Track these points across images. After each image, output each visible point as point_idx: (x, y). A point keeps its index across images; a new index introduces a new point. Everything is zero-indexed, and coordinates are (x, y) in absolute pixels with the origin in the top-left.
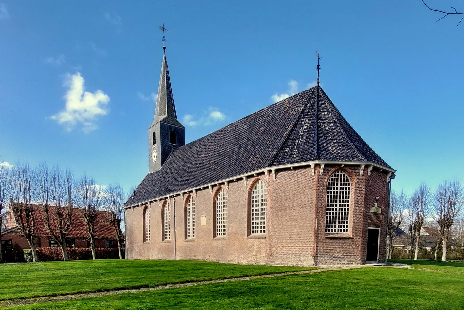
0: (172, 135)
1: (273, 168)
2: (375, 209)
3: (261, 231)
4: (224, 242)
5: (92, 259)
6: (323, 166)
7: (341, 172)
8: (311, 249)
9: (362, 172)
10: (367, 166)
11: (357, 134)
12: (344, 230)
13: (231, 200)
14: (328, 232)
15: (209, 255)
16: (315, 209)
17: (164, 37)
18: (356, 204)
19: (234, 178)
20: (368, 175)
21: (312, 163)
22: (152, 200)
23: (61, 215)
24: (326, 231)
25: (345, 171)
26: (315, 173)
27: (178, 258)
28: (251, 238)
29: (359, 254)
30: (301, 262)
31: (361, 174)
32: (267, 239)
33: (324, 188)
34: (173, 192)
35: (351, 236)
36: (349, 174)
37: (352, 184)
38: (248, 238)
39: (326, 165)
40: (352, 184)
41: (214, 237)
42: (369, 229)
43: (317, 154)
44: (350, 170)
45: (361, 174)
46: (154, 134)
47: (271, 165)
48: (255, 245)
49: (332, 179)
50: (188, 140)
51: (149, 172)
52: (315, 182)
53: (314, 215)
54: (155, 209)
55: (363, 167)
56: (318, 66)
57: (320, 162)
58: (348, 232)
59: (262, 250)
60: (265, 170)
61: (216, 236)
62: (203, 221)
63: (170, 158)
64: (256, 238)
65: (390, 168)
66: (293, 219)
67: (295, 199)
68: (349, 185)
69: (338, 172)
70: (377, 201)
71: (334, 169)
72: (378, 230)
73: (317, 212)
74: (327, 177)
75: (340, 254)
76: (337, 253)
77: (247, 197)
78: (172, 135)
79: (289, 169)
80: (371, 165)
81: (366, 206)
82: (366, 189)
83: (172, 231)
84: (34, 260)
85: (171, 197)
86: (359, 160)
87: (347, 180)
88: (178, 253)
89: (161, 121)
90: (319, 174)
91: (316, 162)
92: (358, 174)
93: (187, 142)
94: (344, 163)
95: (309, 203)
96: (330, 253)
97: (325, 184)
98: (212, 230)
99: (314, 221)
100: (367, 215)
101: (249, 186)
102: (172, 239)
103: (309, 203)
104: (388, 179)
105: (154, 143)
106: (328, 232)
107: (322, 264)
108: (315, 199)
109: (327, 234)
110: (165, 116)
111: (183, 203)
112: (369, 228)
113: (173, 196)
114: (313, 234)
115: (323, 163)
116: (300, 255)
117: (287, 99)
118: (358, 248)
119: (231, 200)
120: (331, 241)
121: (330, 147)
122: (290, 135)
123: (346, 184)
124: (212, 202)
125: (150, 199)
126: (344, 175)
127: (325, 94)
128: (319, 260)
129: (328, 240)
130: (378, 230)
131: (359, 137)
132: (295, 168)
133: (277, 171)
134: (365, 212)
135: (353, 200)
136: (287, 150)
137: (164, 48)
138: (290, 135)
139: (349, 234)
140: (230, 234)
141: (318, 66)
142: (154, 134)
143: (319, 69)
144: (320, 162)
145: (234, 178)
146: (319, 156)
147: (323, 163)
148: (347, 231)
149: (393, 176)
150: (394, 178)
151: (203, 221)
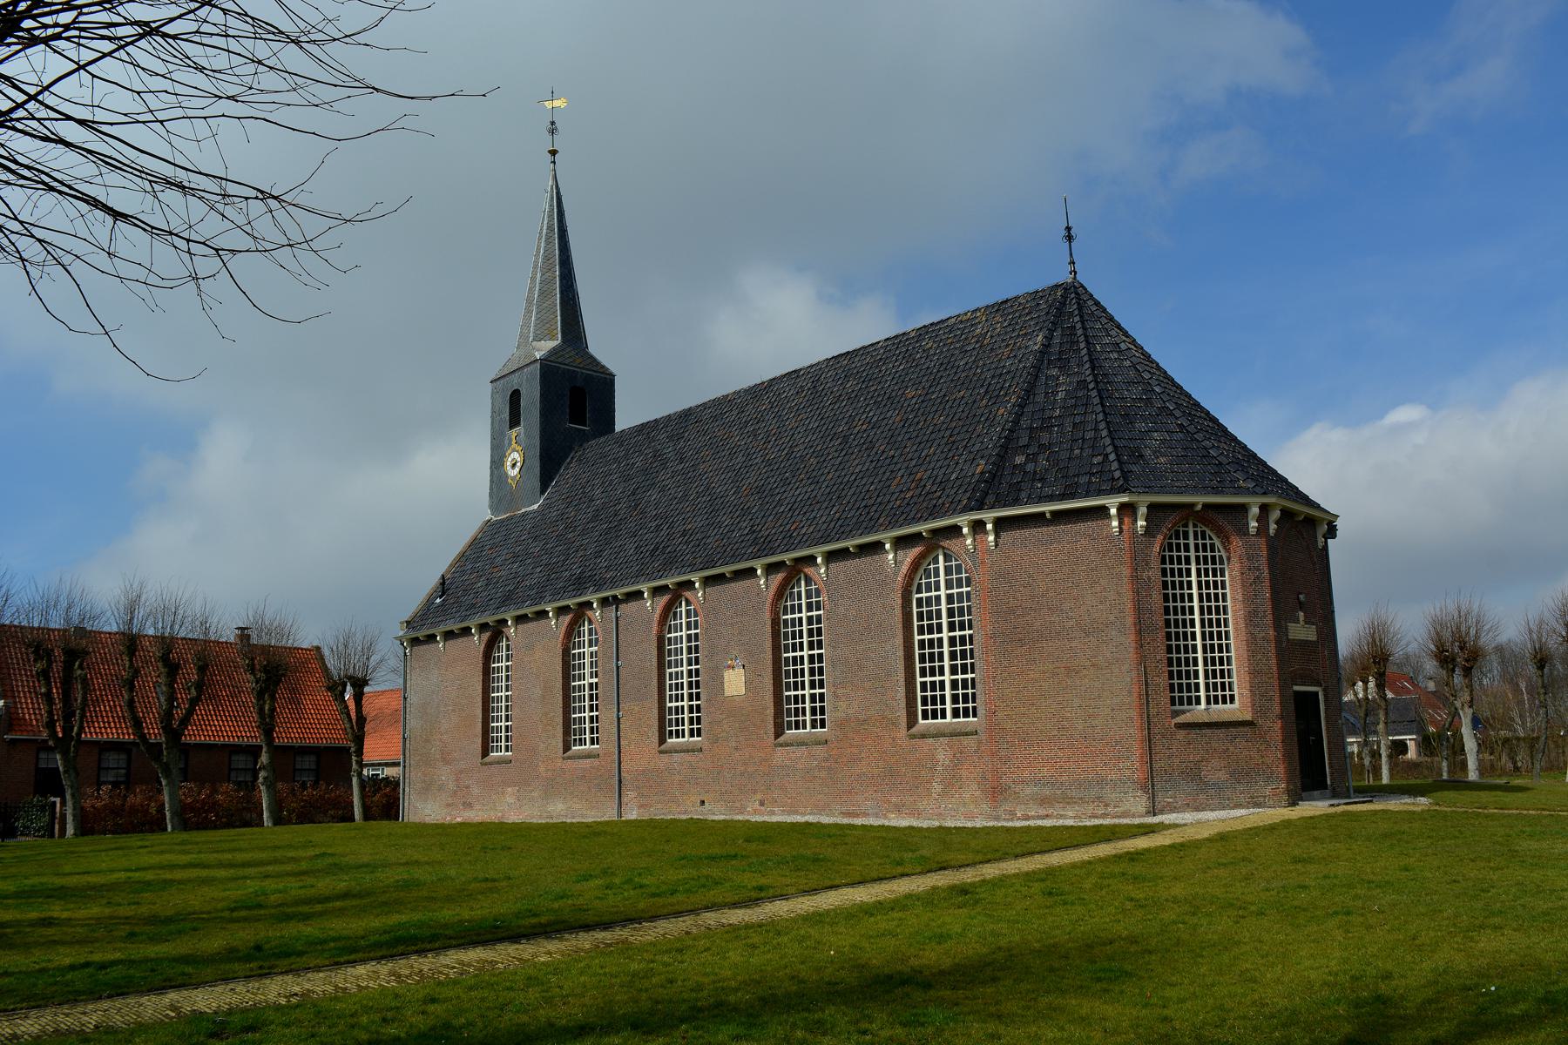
0: (566, 399)
1: (988, 516)
2: (1302, 631)
3: (956, 714)
4: (819, 751)
5: (353, 820)
6: (1143, 510)
7: (1195, 526)
8: (1132, 766)
9: (1253, 524)
10: (1264, 508)
11: (1208, 413)
12: (1224, 697)
13: (842, 610)
14: (1177, 707)
15: (759, 796)
16: (1133, 637)
17: (553, 123)
18: (1251, 617)
19: (850, 544)
20: (1272, 532)
21: (1113, 503)
22: (529, 611)
23: (173, 669)
24: (1173, 704)
25: (1206, 522)
26: (1121, 531)
27: (632, 814)
28: (923, 736)
29: (1281, 770)
30: (1106, 805)
31: (1252, 531)
32: (983, 737)
33: (1154, 574)
34: (614, 583)
35: (1248, 717)
36: (1220, 532)
37: (1229, 559)
38: (913, 737)
39: (1152, 507)
40: (1229, 559)
41: (909, 728)
42: (1297, 693)
43: (1117, 474)
44: (1221, 521)
45: (1252, 531)
46: (515, 395)
47: (980, 507)
48: (940, 756)
49: (1170, 545)
50: (628, 414)
51: (488, 516)
52: (1127, 558)
53: (1131, 654)
54: (532, 650)
55: (1255, 510)
56: (1068, 229)
57: (1134, 498)
58: (1236, 705)
59: (964, 774)
60: (963, 521)
61: (783, 733)
62: (734, 682)
63: (570, 473)
64: (944, 735)
65: (1317, 506)
66: (1067, 668)
67: (1066, 606)
68: (1222, 563)
69: (1186, 525)
70: (1301, 606)
71: (1174, 517)
72: (1316, 694)
73: (1140, 645)
74: (1160, 537)
75: (1222, 775)
76: (1215, 772)
77: (900, 602)
78: (566, 399)
79: (1038, 519)
80: (1276, 504)
81: (1280, 625)
82: (1271, 572)
83: (607, 716)
84: (70, 830)
85: (604, 602)
86: (1239, 491)
87: (1213, 546)
88: (630, 795)
89: (544, 362)
90: (1134, 531)
91: (1125, 499)
92: (1243, 531)
93: (618, 428)
94: (1200, 500)
95: (1112, 618)
96: (1193, 774)
97: (1155, 563)
98: (771, 711)
99: (1134, 674)
100: (1287, 650)
101: (904, 569)
102: (607, 746)
103: (1112, 618)
104: (1321, 540)
105: (514, 421)
106: (1177, 707)
107: (1173, 810)
108: (1129, 605)
109: (1176, 714)
110: (551, 344)
111: (650, 622)
112: (1296, 688)
113: (615, 597)
114: (1134, 713)
115: (1143, 502)
116: (1101, 782)
117: (978, 309)
118: (1273, 753)
119: (842, 610)
120: (1194, 733)
121: (1148, 452)
122: (1019, 416)
123: (1213, 558)
124: (767, 617)
125: (520, 603)
126: (1203, 533)
127: (1097, 303)
128: (1164, 799)
129: (1183, 732)
130: (1316, 694)
131: (1215, 420)
132: (1059, 517)
133: (1000, 524)
134: (1278, 641)
135: (1240, 606)
136: (1019, 460)
137: (553, 153)
138: (1019, 416)
139: (1237, 708)
140: (841, 724)
141: (1068, 229)
142: (515, 395)
143: (1070, 238)
144: (1134, 498)
145: (850, 544)
146: (1125, 475)
147: (1143, 502)
148: (1232, 698)
149: (1332, 532)
150: (1334, 537)
151: (734, 682)
